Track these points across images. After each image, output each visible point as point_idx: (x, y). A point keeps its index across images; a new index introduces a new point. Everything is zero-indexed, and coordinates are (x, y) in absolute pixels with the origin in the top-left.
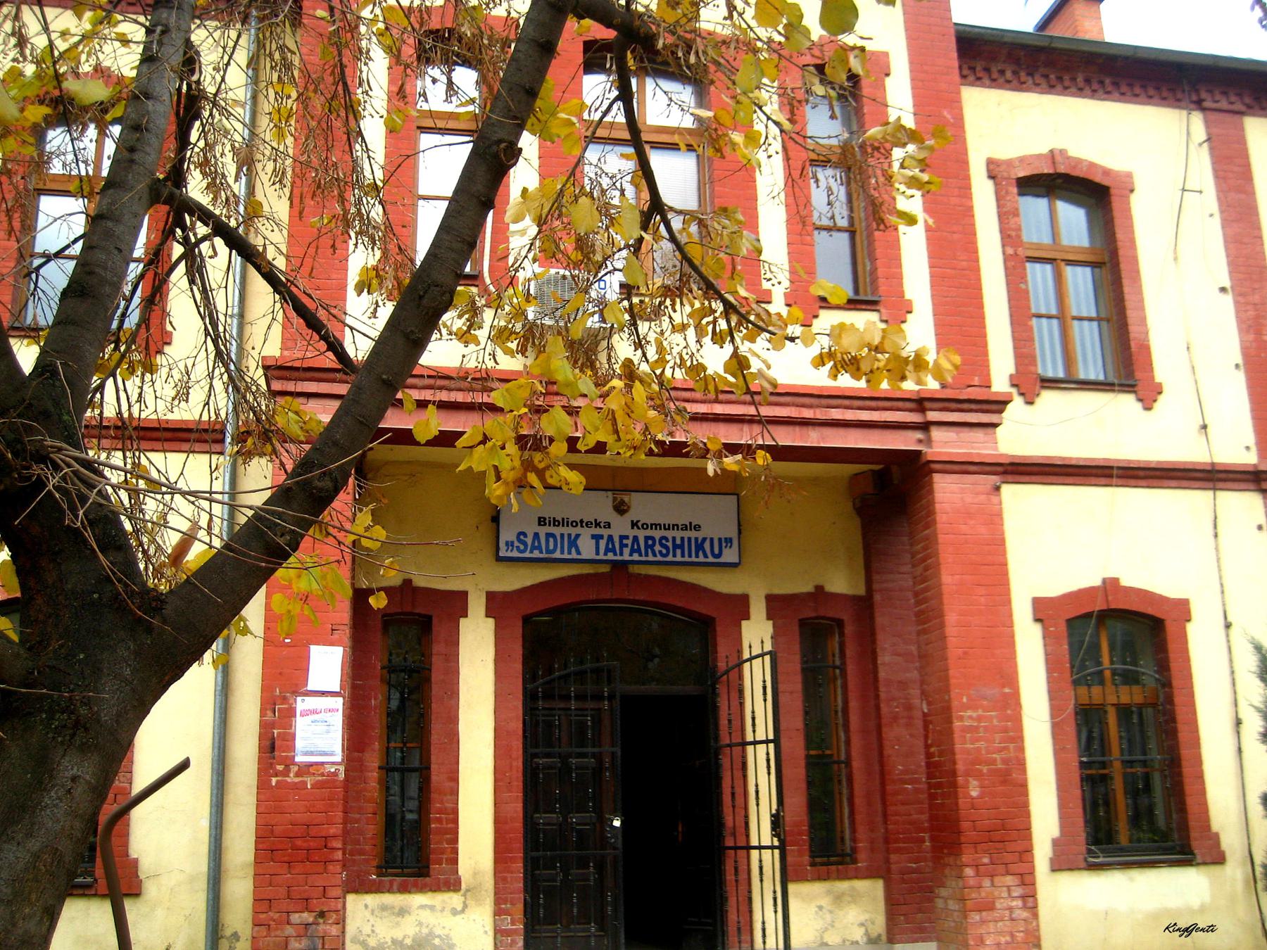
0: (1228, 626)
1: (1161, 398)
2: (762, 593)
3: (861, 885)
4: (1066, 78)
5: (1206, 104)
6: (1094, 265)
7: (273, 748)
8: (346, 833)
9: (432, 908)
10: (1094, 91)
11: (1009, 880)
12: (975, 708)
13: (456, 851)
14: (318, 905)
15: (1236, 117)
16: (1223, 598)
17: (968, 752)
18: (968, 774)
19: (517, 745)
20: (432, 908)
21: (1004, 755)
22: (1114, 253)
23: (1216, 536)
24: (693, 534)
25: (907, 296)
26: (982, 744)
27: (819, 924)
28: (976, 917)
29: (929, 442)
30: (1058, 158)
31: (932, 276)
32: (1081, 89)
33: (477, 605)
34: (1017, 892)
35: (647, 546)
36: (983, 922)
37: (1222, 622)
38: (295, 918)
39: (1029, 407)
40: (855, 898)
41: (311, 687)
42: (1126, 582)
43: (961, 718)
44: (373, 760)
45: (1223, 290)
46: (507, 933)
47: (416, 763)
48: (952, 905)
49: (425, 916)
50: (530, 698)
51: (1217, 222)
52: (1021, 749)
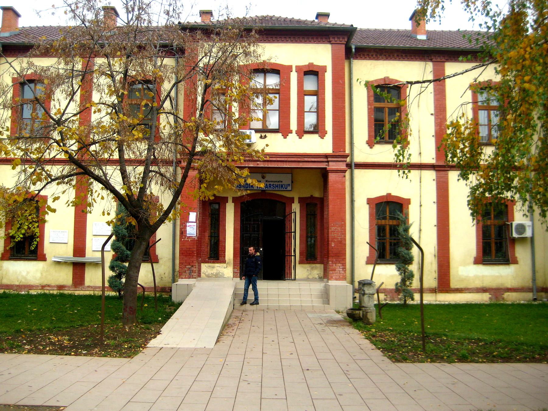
0: (421, 206)
2: (298, 197)
3: (318, 265)
4: (391, 55)
5: (433, 60)
7: (182, 233)
8: (197, 250)
9: (220, 267)
10: (400, 59)
11: (340, 265)
12: (335, 227)
13: (225, 255)
14: (191, 264)
15: (442, 63)
16: (420, 199)
17: (332, 236)
18: (332, 241)
19: (239, 232)
20: (220, 267)
21: (341, 237)
23: (420, 182)
24: (281, 183)
25: (326, 130)
26: (336, 235)
27: (307, 274)
28: (331, 272)
29: (328, 165)
30: (386, 80)
31: (333, 124)
32: (395, 58)
33: (230, 200)
34: (341, 267)
35: (269, 186)
36: (333, 273)
37: (419, 204)
38: (187, 267)
39: (371, 149)
40: (316, 268)
41: (190, 221)
42: (393, 194)
43: (331, 229)
44: (207, 234)
45: (432, 114)
46: (236, 273)
47: (216, 235)
49: (218, 268)
50: (242, 221)
51: (432, 95)
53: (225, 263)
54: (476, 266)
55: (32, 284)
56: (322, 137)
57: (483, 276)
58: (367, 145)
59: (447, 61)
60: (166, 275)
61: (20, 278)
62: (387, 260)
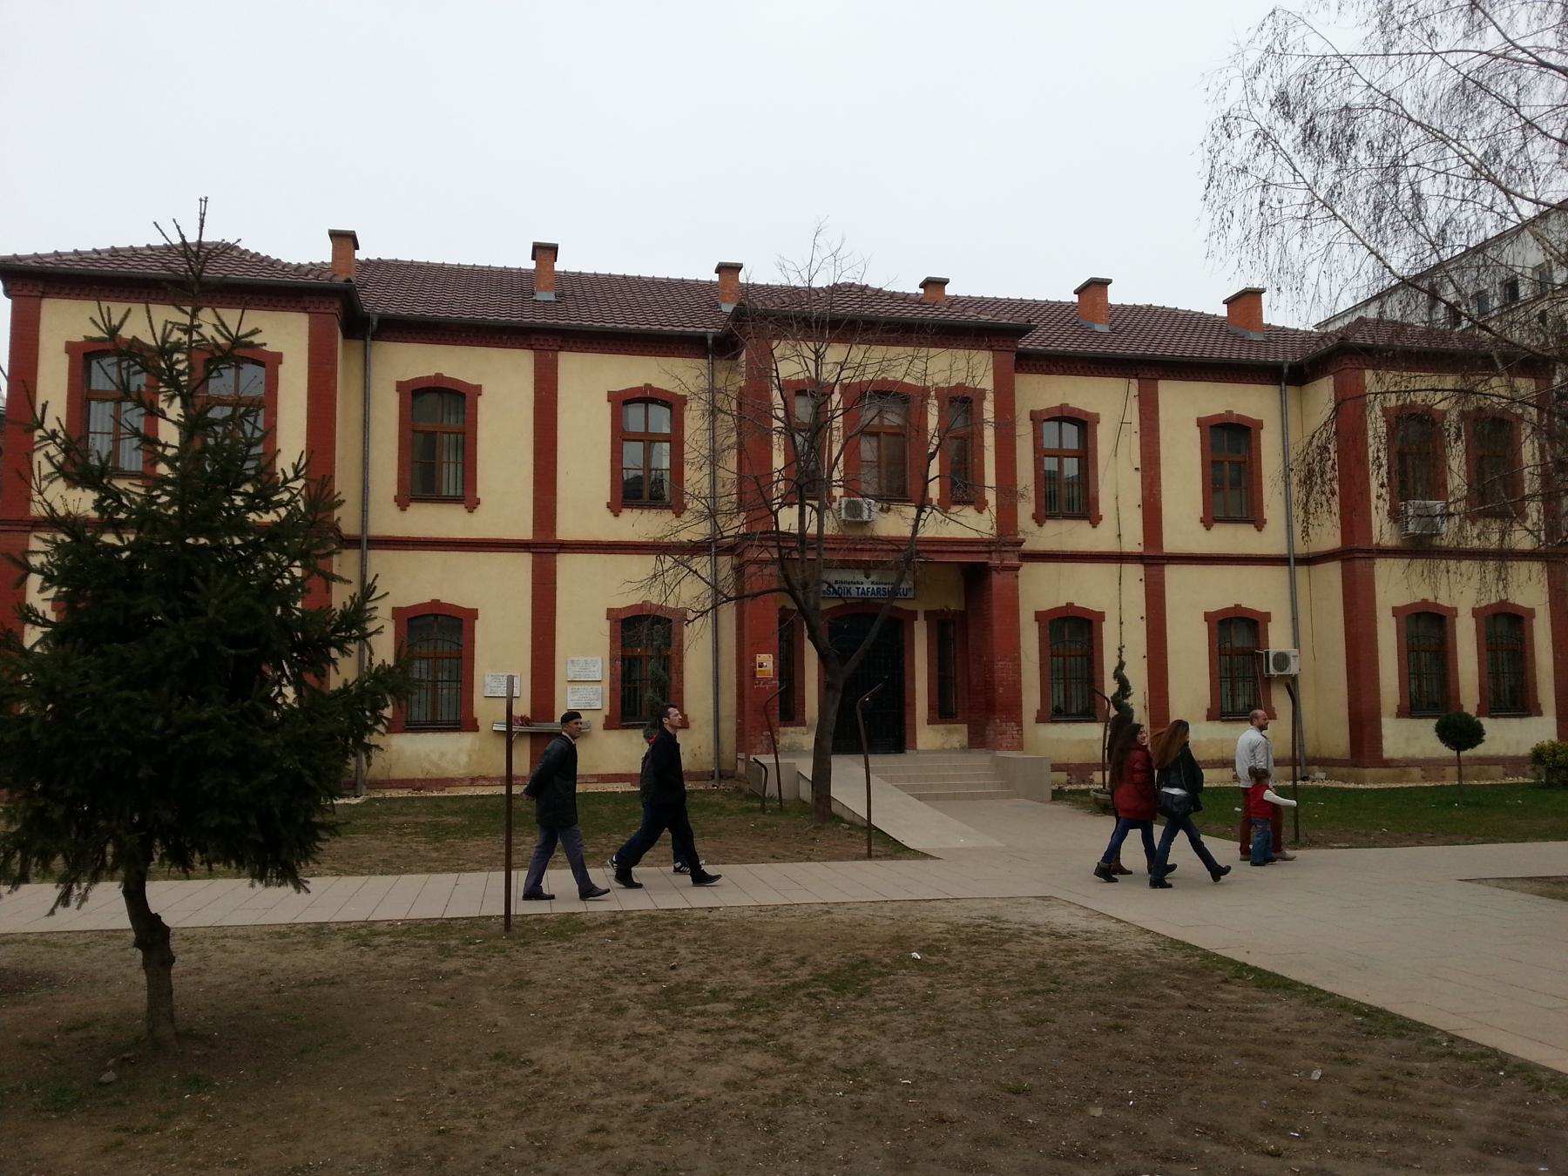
0: (1121, 623)
1: (1101, 523)
6: (1079, 457)
11: (1013, 724)
22: (1087, 453)
29: (990, 558)
48: (992, 732)
49: (793, 735)
52: (1020, 676)
53: (805, 725)
54: (1210, 724)
55: (451, 776)
56: (980, 511)
57: (1222, 741)
58: (608, 510)
59: (1162, 377)
60: (703, 749)
61: (427, 765)
62: (1073, 715)
